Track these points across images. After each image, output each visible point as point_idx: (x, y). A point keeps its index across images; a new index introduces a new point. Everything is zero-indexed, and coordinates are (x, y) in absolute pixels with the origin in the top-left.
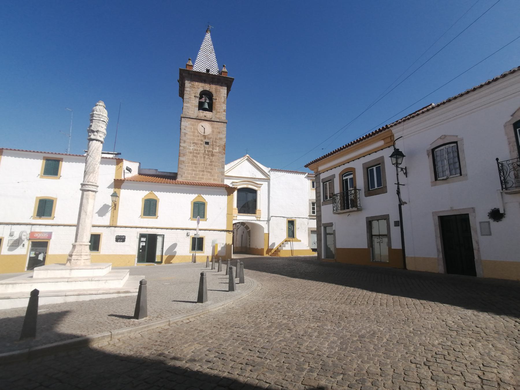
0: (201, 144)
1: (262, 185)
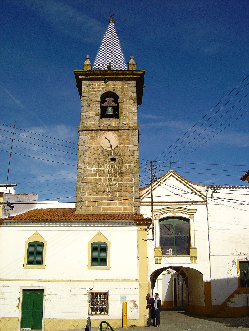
1: (196, 210)
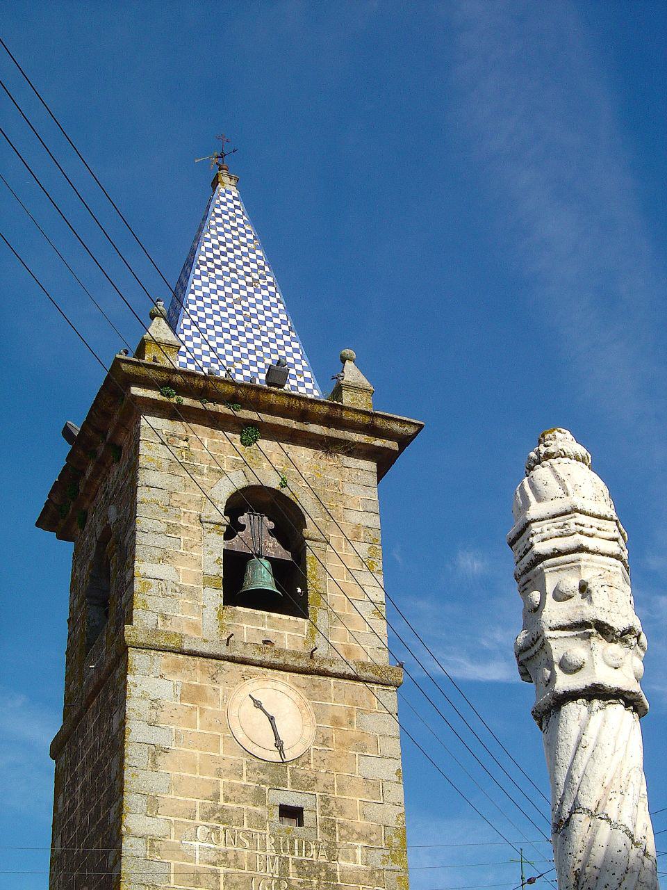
0: (260, 822)
